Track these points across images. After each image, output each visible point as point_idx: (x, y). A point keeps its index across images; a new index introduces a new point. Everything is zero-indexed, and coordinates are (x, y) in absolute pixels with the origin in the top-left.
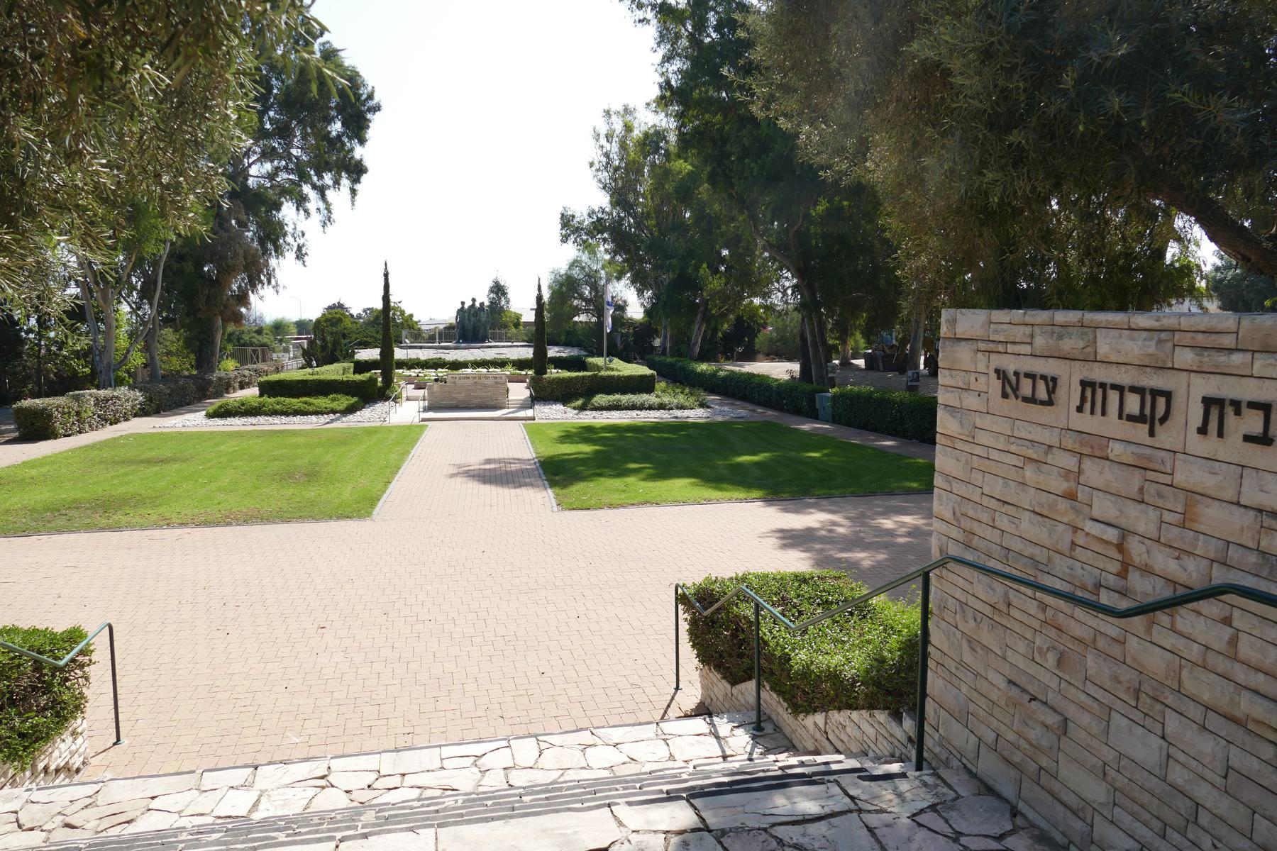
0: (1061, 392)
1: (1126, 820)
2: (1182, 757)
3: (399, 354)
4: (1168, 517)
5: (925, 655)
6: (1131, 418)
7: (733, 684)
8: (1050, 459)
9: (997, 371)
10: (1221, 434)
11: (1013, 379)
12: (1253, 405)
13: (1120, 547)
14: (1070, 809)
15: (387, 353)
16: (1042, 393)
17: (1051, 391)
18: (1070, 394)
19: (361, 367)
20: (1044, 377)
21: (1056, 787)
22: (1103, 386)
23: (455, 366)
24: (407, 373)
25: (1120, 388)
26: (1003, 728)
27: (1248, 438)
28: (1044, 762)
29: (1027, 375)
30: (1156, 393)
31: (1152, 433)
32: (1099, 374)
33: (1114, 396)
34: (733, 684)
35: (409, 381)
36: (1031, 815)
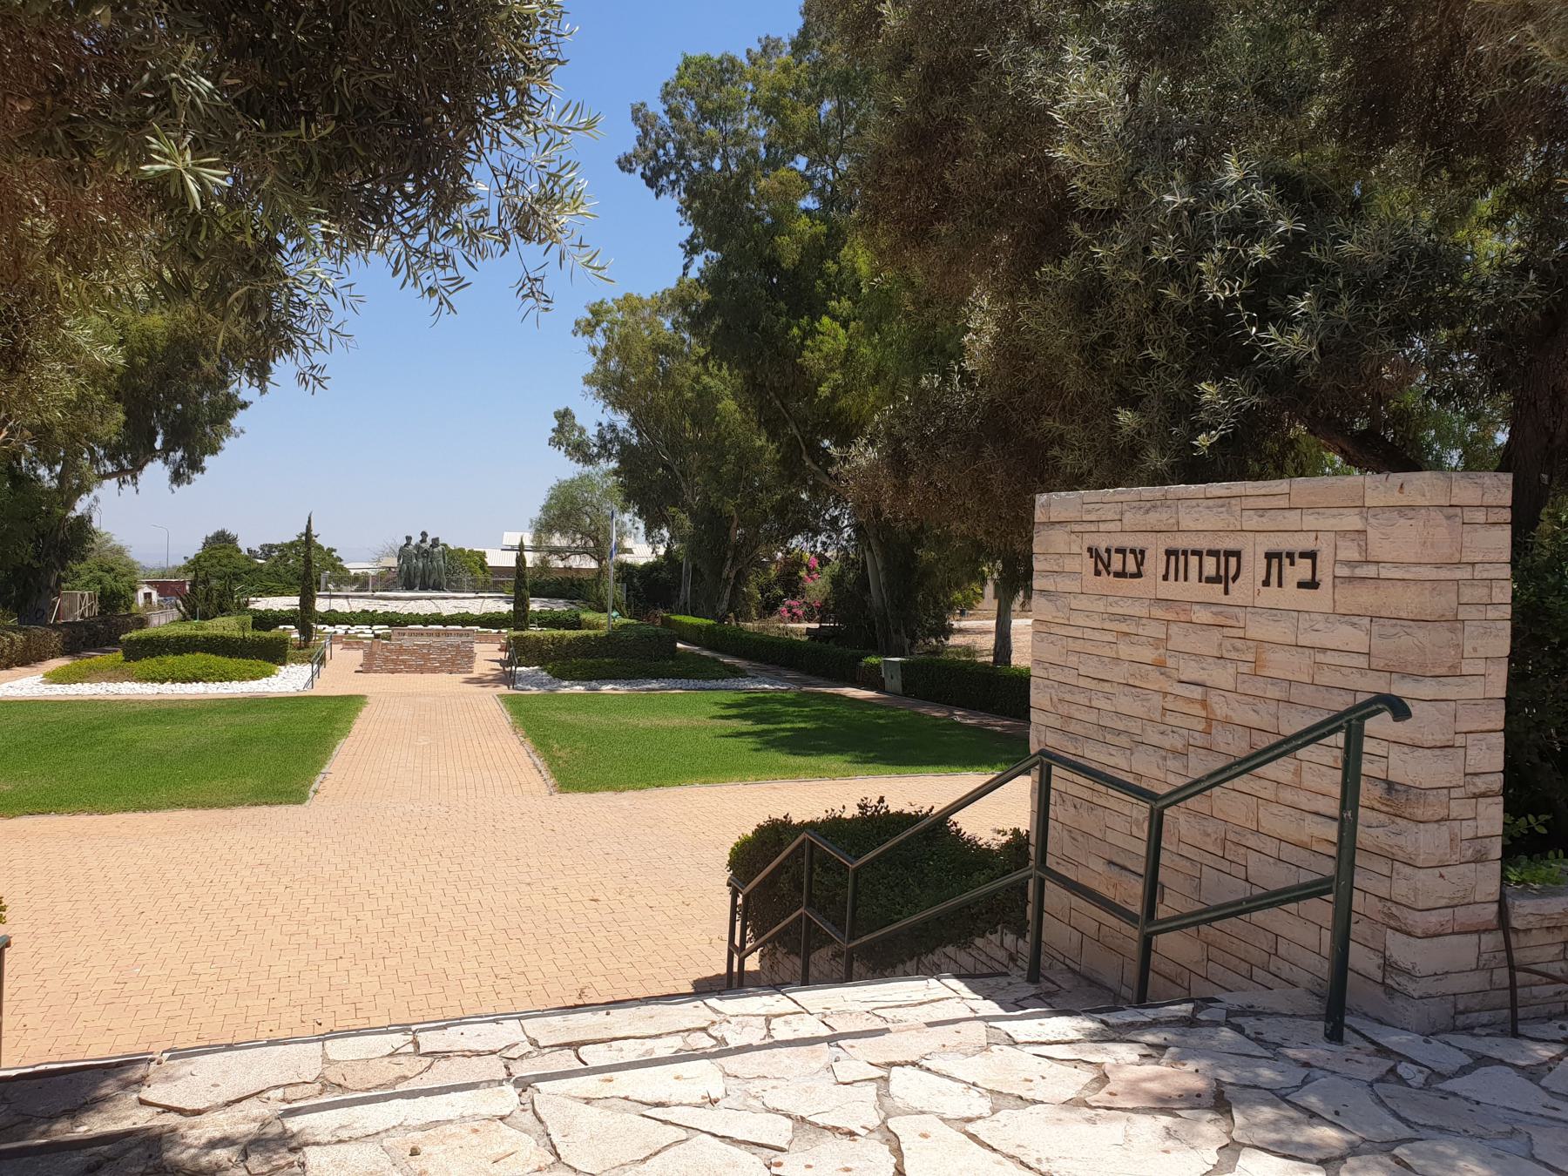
6: (1209, 580)
11: (1105, 556)
12: (1303, 555)
16: (1131, 567)
17: (1139, 564)
19: (265, 621)
22: (1185, 553)
23: (392, 620)
24: (329, 629)
27: (1301, 585)
31: (1226, 592)
33: (1194, 560)
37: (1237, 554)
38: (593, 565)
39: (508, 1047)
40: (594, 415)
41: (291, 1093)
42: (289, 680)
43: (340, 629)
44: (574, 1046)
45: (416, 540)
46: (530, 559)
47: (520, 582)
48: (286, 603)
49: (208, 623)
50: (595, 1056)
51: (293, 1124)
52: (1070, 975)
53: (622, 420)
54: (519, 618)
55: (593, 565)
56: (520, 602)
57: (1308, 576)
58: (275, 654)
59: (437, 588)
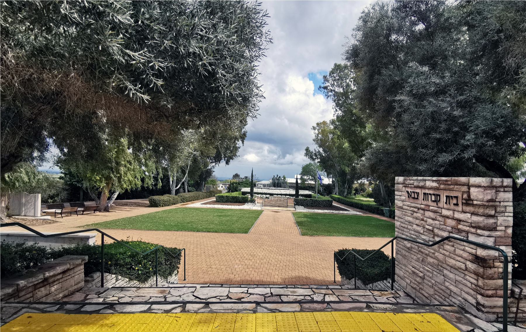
0: (420, 195)
1: (437, 297)
2: (447, 280)
3: (255, 190)
4: (441, 223)
5: (394, 264)
6: (433, 201)
7: (350, 280)
8: (418, 211)
9: (407, 191)
10: (449, 204)
11: (410, 193)
12: (455, 197)
13: (433, 231)
14: (426, 297)
15: (252, 190)
16: (416, 197)
17: (418, 196)
18: (421, 197)
19: (244, 193)
20: (416, 192)
21: (423, 292)
22: (428, 194)
23: (271, 195)
24: (257, 195)
25: (430, 194)
26: (412, 279)
27: (454, 204)
28: (421, 286)
29: (413, 192)
30: (437, 195)
31: (437, 204)
32: (427, 191)
33: (430, 196)
34: (350, 280)
35: (258, 198)
36: (419, 301)
37: (439, 195)
38: (314, 183)
39: (266, 294)
40: (314, 148)
41: (221, 298)
42: (247, 206)
43: (259, 195)
44: (280, 296)
45: (276, 176)
46: (299, 181)
47: (297, 187)
48: (248, 190)
49: (233, 193)
50: (284, 299)
51: (411, 272)
52: (403, 293)
53: (321, 150)
54: (297, 195)
55: (314, 183)
56: (297, 192)
57: (456, 203)
58: (243, 201)
59: (281, 187)
